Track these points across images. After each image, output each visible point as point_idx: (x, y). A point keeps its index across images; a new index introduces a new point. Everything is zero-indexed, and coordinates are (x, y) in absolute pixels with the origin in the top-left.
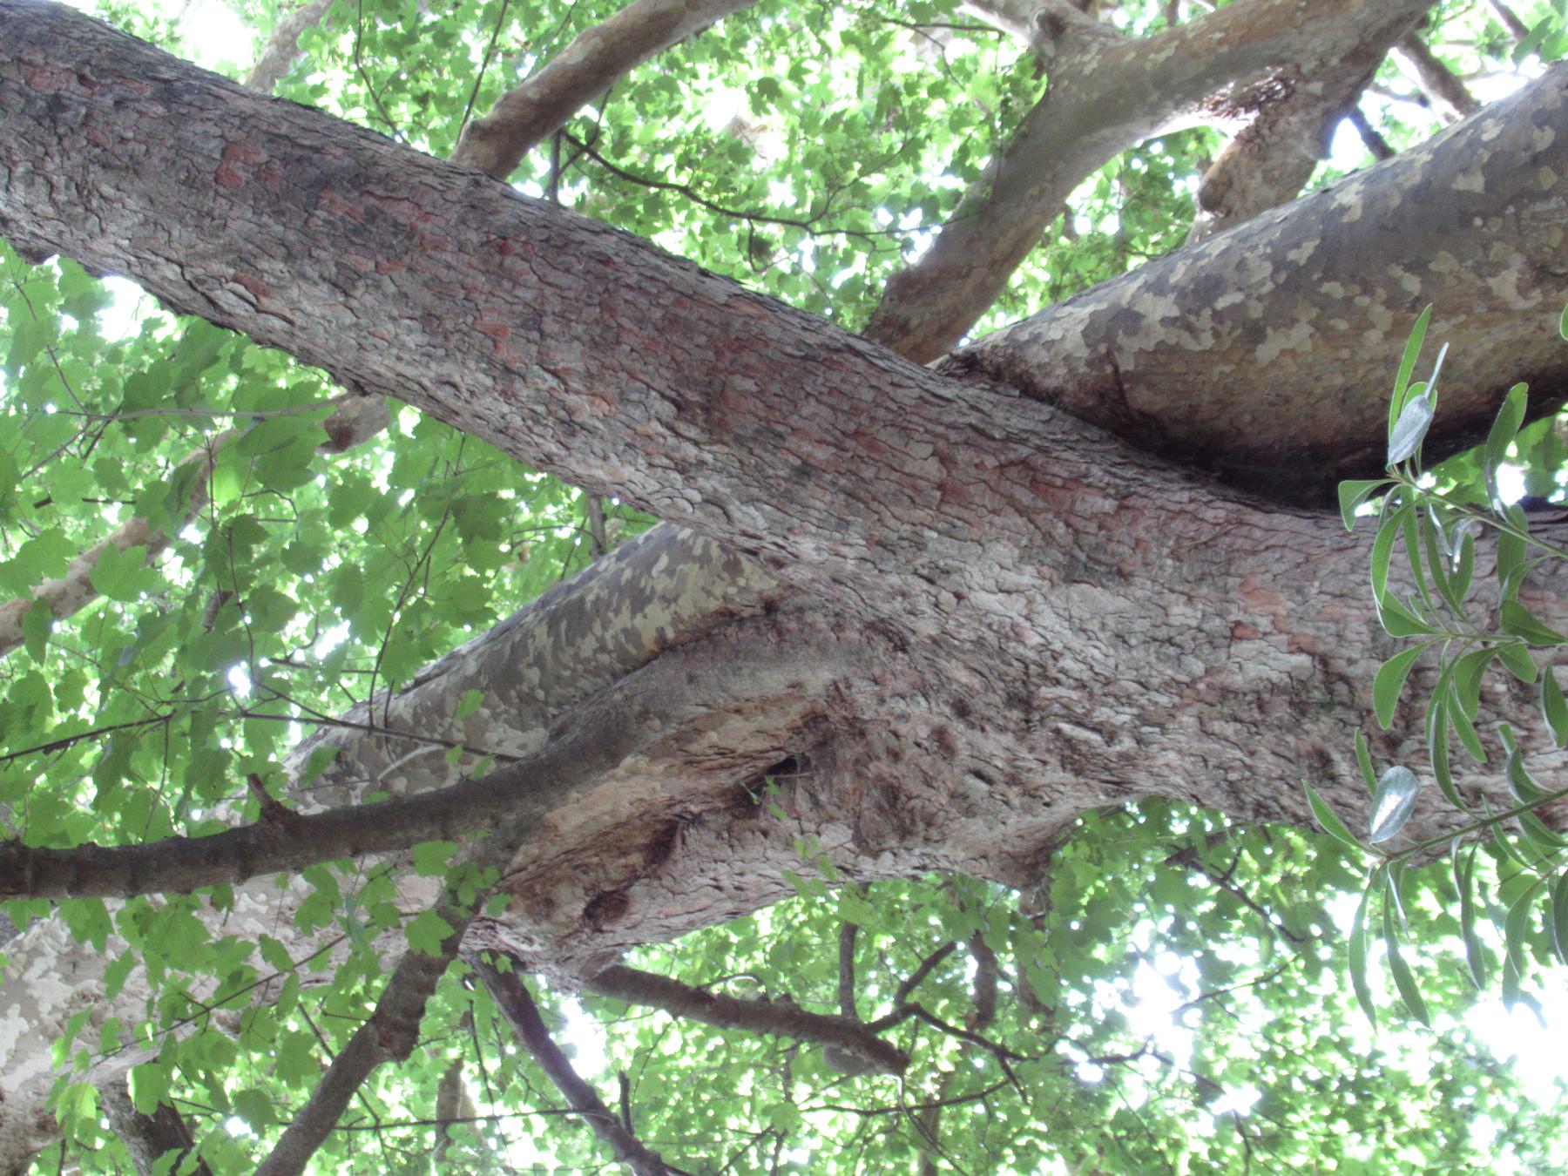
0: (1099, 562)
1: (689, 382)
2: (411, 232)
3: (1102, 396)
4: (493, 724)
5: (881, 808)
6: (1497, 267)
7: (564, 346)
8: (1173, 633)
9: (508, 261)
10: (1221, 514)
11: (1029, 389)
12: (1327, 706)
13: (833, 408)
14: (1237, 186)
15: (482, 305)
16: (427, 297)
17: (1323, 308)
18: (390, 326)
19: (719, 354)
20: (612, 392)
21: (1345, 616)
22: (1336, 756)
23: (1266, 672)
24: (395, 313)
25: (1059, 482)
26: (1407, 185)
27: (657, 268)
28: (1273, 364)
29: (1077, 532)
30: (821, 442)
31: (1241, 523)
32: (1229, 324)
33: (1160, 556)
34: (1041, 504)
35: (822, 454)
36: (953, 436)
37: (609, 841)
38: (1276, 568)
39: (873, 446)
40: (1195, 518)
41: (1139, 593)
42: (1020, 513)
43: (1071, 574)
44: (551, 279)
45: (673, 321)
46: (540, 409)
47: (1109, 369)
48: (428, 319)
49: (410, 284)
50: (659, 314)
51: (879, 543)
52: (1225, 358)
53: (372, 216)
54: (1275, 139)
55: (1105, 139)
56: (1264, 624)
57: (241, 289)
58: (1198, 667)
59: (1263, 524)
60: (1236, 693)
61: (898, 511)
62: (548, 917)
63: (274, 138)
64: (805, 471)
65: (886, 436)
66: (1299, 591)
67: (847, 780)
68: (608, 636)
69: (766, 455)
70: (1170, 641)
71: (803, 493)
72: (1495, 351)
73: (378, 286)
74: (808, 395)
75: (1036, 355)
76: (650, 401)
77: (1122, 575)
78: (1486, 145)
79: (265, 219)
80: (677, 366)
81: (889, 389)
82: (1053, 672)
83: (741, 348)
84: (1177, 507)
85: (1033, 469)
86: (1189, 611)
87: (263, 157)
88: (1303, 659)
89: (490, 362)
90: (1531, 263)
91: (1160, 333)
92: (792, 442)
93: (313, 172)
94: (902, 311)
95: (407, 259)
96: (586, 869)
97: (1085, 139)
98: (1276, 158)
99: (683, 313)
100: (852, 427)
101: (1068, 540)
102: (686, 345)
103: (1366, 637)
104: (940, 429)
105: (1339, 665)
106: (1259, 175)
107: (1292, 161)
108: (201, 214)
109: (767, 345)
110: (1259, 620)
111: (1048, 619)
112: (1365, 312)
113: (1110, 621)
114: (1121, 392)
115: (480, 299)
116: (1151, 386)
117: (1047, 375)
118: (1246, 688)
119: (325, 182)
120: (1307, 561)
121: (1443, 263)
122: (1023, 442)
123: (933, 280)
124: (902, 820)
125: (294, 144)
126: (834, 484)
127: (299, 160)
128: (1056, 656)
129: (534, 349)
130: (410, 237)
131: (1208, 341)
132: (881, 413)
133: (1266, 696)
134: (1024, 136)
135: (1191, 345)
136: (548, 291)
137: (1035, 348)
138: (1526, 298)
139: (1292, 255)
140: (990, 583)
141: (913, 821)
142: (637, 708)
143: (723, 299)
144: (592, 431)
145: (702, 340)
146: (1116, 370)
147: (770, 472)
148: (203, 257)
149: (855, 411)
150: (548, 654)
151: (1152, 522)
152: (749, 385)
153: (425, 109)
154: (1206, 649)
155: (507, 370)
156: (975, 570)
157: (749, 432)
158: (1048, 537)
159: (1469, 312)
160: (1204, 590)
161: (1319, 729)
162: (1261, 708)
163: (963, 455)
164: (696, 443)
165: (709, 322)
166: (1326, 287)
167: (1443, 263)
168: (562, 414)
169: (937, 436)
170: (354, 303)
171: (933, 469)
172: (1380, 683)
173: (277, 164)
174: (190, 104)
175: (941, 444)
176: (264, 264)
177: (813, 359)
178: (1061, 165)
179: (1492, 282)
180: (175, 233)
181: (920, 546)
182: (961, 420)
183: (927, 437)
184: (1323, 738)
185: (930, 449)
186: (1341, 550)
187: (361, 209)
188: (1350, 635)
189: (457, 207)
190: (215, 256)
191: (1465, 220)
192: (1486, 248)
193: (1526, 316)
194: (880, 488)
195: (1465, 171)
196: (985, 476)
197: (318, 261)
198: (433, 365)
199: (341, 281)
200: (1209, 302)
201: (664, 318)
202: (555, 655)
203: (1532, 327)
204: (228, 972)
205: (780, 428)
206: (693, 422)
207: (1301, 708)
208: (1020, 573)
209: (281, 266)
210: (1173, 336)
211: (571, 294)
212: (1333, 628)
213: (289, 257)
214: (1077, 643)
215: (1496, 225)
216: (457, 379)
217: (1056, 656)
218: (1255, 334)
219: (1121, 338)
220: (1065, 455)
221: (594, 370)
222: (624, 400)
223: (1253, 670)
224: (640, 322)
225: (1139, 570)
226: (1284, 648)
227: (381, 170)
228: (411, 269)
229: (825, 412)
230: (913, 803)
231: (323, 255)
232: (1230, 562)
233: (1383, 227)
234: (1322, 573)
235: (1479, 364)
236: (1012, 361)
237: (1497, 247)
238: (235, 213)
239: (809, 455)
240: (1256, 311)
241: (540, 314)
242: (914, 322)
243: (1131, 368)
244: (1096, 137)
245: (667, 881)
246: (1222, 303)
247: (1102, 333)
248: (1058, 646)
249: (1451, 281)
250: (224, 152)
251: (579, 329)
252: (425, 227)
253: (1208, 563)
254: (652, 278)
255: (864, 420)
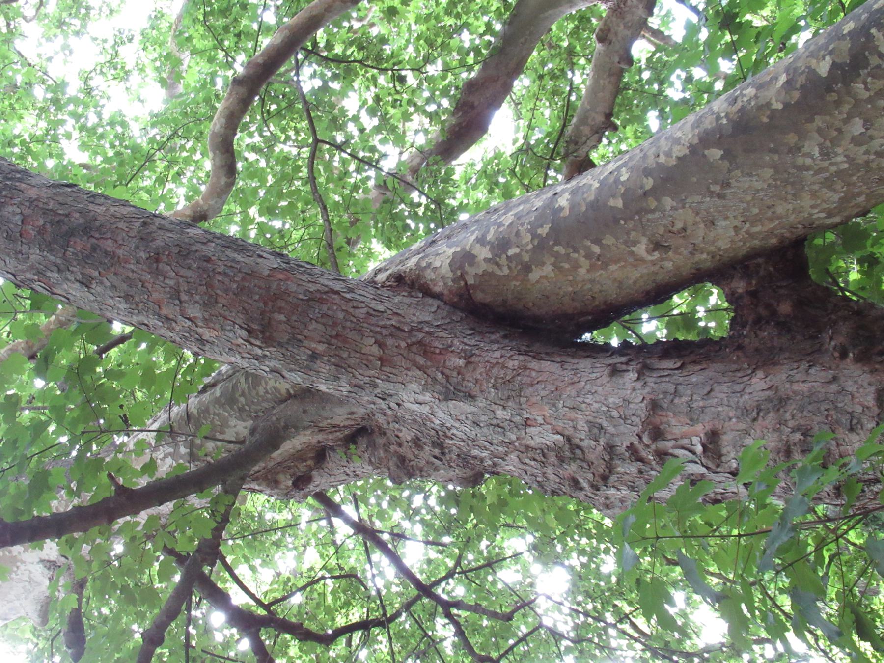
0: (459, 391)
1: (252, 319)
2: (113, 256)
3: (461, 296)
4: (230, 419)
5: (398, 466)
6: (635, 243)
7: (191, 306)
8: (499, 422)
9: (160, 265)
10: (516, 363)
11: (427, 292)
12: (574, 459)
13: (324, 324)
14: (612, 30)
15: (150, 289)
16: (125, 286)
17: (556, 258)
18: (111, 300)
19: (266, 304)
20: (217, 326)
21: (576, 418)
22: (581, 480)
23: (544, 441)
24: (112, 295)
25: (437, 351)
26: (589, 200)
27: (234, 260)
28: (537, 282)
29: (447, 377)
30: (320, 342)
31: (526, 368)
32: (514, 262)
33: (488, 387)
34: (429, 364)
35: (321, 348)
36: (385, 332)
37: (298, 456)
38: (543, 393)
39: (345, 340)
40: (504, 367)
41: (480, 404)
42: (420, 369)
43: (447, 397)
44: (181, 273)
45: (242, 289)
46: (186, 335)
47: (462, 283)
48: (127, 297)
49: (116, 281)
50: (235, 286)
51: (355, 386)
52: (515, 278)
53: (94, 248)
54: (627, 9)
55: (551, 15)
56: (540, 420)
57: (43, 285)
58: (514, 437)
59: (536, 368)
60: (533, 448)
61: (361, 372)
62: (276, 487)
63: (45, 212)
64: (314, 356)
65: (352, 335)
66: (554, 405)
67: (382, 453)
68: (268, 387)
69: (294, 350)
70: (498, 426)
71: (316, 366)
72: (641, 277)
73: (102, 283)
74: (312, 319)
75: (430, 275)
76: (236, 330)
77: (471, 397)
78: (622, 183)
79: (45, 254)
80: (246, 311)
81: (351, 310)
82: (449, 434)
83: (276, 299)
84: (494, 361)
85: (425, 345)
86: (505, 413)
87: (41, 222)
88: (559, 437)
89: (159, 316)
90: (650, 241)
91: (484, 266)
92: (306, 343)
93: (65, 228)
94: (471, 98)
95: (113, 269)
96: (289, 468)
97: (542, 16)
98: (628, 17)
99: (247, 284)
100: (334, 333)
101: (444, 381)
102: (250, 301)
103: (586, 429)
104: (378, 329)
105: (576, 441)
106: (622, 27)
107: (636, 18)
108: (17, 253)
109: (289, 295)
110: (537, 418)
111: (440, 414)
112: (576, 261)
113: (469, 416)
114: (470, 295)
115: (149, 286)
116: (483, 291)
117: (435, 285)
118: (536, 447)
119: (71, 233)
120: (557, 389)
121: (609, 240)
122: (419, 330)
123: (482, 84)
124: (408, 470)
125: (56, 213)
126: (329, 361)
127: (58, 222)
128: (449, 429)
129: (178, 308)
130: (113, 258)
131: (506, 271)
132: (348, 324)
133: (546, 451)
134: (515, 15)
135: (499, 272)
136: (181, 280)
137: (429, 271)
138: (651, 255)
139: (539, 231)
140: (412, 400)
141: (414, 471)
142: (282, 424)
143: (266, 273)
144: (212, 343)
145: (257, 297)
146: (466, 283)
147: (298, 357)
148: (23, 271)
149: (335, 324)
150: (246, 391)
151: (483, 370)
152: (282, 317)
153: (240, 39)
154: (515, 430)
155: (167, 319)
156: (404, 394)
157: (285, 340)
158: (434, 379)
159: (625, 261)
160: (510, 404)
161: (572, 468)
162: (544, 456)
163: (390, 342)
164: (260, 348)
165: (260, 288)
166: (556, 248)
167: (609, 240)
168: (197, 336)
169: (377, 333)
170: (93, 291)
171: (375, 350)
172: (595, 450)
173: (48, 226)
174: (6, 196)
175: (379, 337)
176: (49, 274)
177: (313, 300)
178: (532, 28)
179: (634, 249)
180: (8, 261)
181: (375, 386)
182: (388, 323)
183: (371, 334)
184: (574, 472)
185: (373, 340)
186: (573, 383)
187: (89, 245)
188: (579, 427)
189: (134, 240)
190: (27, 271)
191: (616, 221)
192: (628, 234)
193: (654, 263)
194: (352, 361)
195: (614, 196)
196: (402, 352)
197: (72, 272)
198: (134, 317)
199: (85, 281)
200: (505, 251)
201: (237, 288)
202: (249, 393)
203: (657, 267)
204: (129, 536)
205: (299, 337)
206: (257, 338)
207: (561, 460)
208: (424, 395)
209: (57, 275)
210: (491, 268)
211: (192, 281)
212: (571, 424)
213: (59, 271)
214: (457, 425)
215: (631, 224)
216: (146, 322)
217: (449, 429)
218: (527, 268)
219: (467, 268)
220: (441, 334)
221: (207, 317)
222: (223, 329)
223: (538, 440)
224: (226, 291)
225: (479, 394)
226: (550, 431)
227: (98, 223)
228: (116, 274)
229: (320, 327)
230: (412, 463)
231: (75, 269)
232: (521, 390)
233: (579, 221)
234: (564, 396)
235: (635, 282)
236: (419, 277)
237: (633, 234)
238: (31, 251)
239: (315, 348)
240: (526, 258)
241: (178, 292)
242: (476, 103)
243: (473, 282)
244: (546, 14)
245: (326, 470)
246: (510, 252)
247: (458, 264)
248: (448, 425)
249: (614, 248)
250: (22, 222)
251: (197, 298)
252: (120, 252)
253: (511, 390)
254: (231, 267)
255: (340, 328)
